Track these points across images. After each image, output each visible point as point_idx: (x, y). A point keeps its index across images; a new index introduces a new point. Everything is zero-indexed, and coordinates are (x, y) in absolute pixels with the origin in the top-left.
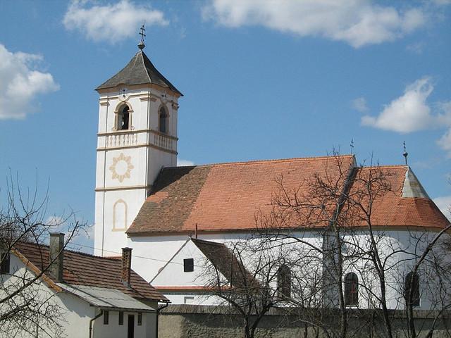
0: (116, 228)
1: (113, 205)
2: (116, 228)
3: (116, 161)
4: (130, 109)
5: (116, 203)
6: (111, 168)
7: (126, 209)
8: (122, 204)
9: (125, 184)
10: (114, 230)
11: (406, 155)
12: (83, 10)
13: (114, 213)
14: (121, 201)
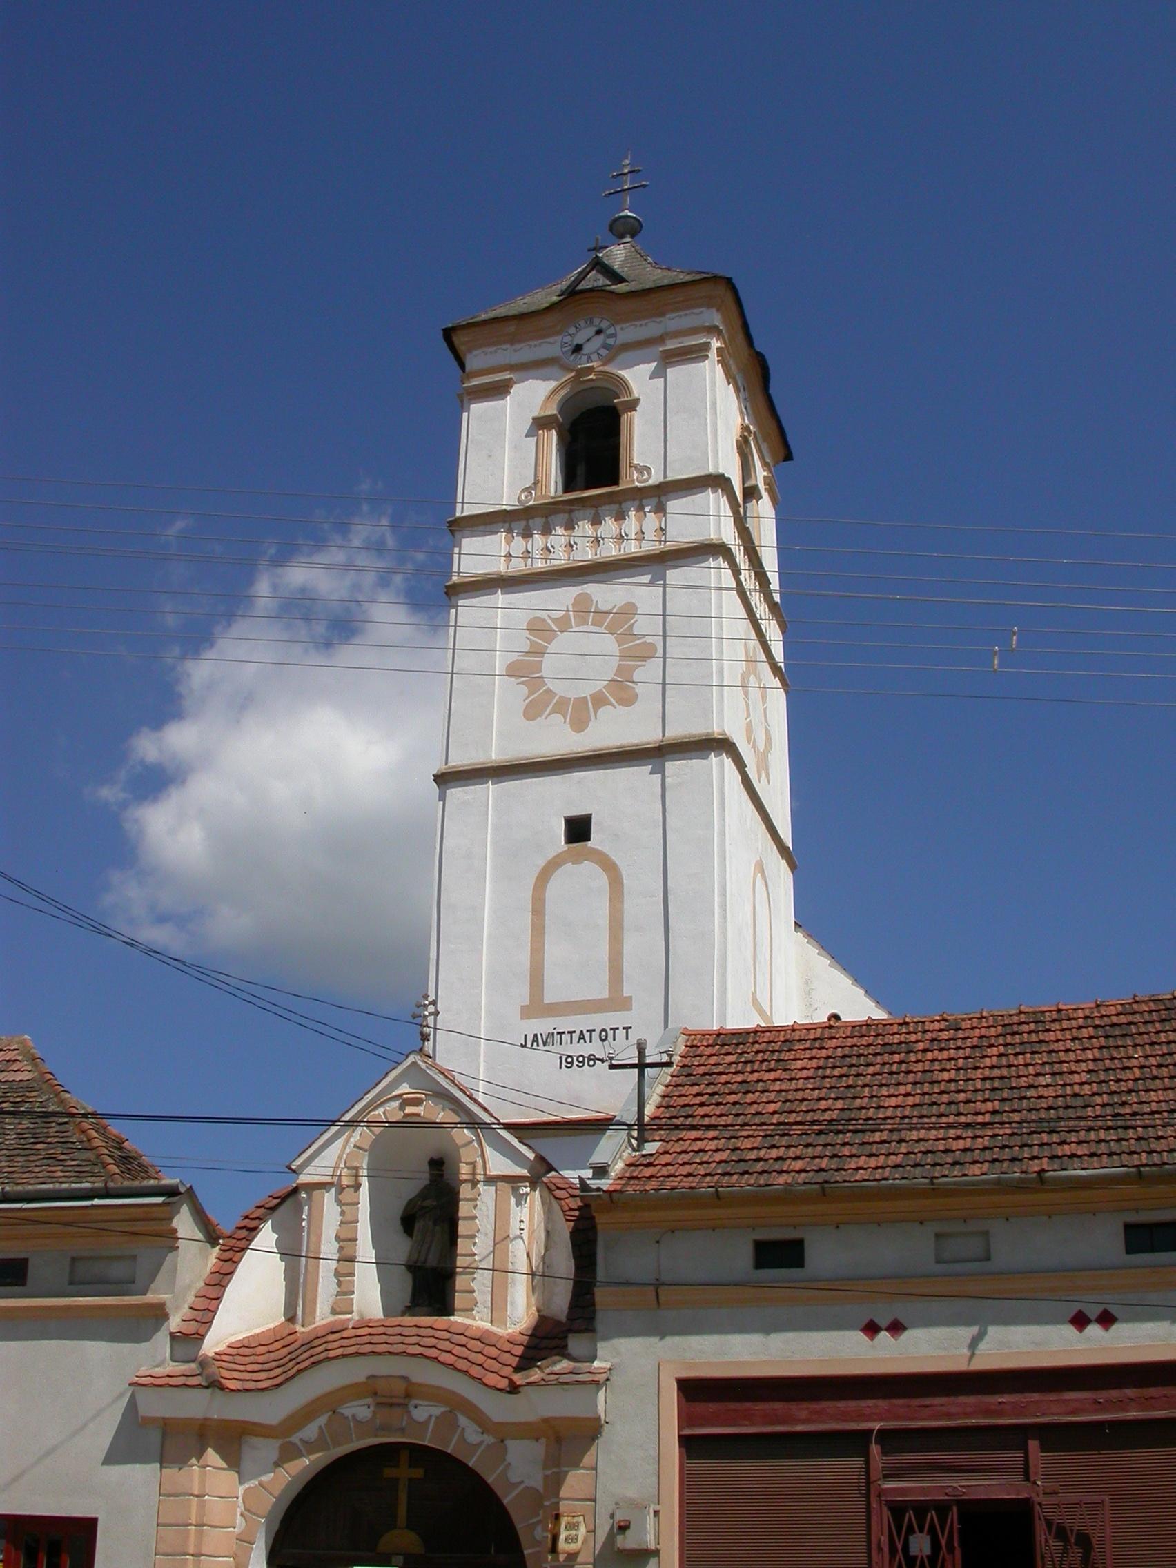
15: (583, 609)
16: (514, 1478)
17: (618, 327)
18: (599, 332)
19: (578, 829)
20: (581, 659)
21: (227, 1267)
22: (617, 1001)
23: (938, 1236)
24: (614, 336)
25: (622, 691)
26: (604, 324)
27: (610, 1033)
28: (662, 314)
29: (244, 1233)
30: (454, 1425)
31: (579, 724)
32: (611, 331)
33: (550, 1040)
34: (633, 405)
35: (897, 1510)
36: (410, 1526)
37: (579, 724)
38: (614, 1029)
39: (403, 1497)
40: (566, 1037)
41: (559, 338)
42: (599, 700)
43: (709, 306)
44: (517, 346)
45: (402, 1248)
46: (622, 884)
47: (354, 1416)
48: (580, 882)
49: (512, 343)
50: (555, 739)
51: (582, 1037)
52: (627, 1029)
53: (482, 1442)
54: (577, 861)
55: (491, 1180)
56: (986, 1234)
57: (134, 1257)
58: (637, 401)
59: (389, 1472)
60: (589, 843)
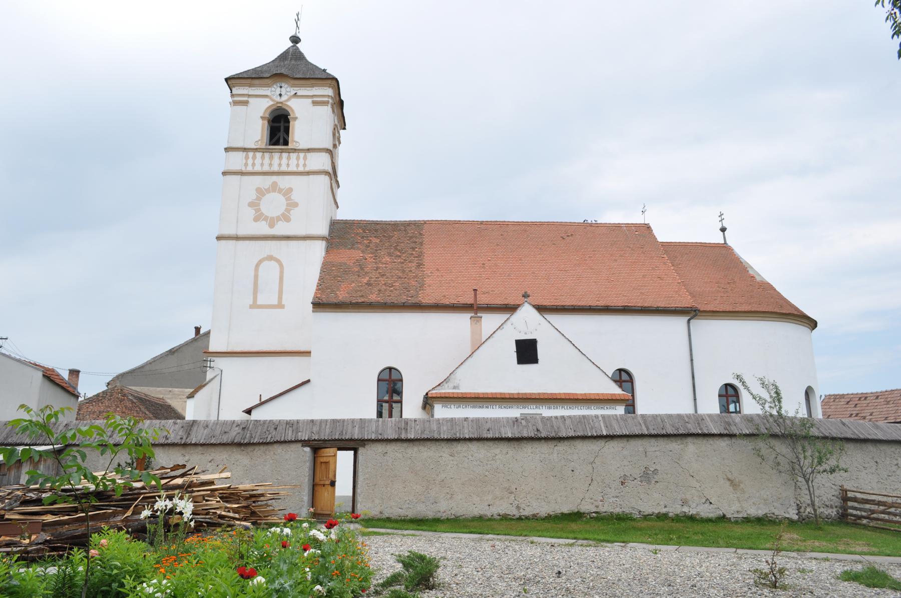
0: (259, 302)
1: (256, 262)
2: (259, 302)
3: (261, 192)
4: (292, 116)
5: (257, 266)
6: (272, 226)
7: (282, 272)
8: (273, 263)
9: (281, 229)
10: (254, 306)
11: (723, 230)
12: (582, 511)
13: (256, 277)
14: (270, 258)
31: (272, 226)
34: (296, 118)
42: (278, 219)
50: (262, 229)
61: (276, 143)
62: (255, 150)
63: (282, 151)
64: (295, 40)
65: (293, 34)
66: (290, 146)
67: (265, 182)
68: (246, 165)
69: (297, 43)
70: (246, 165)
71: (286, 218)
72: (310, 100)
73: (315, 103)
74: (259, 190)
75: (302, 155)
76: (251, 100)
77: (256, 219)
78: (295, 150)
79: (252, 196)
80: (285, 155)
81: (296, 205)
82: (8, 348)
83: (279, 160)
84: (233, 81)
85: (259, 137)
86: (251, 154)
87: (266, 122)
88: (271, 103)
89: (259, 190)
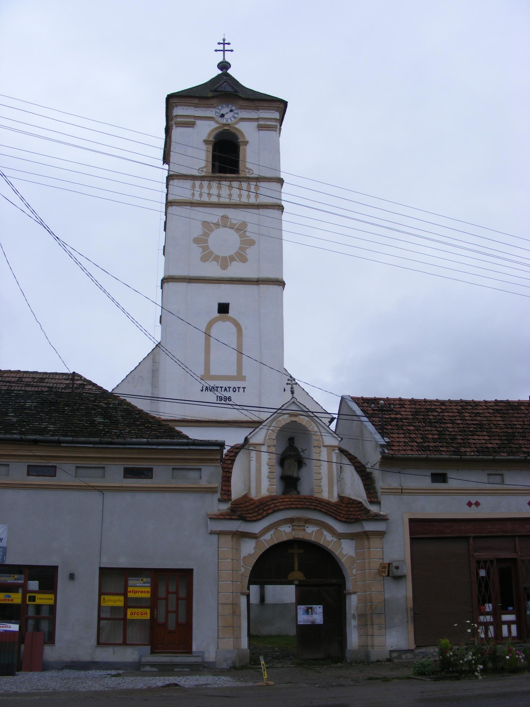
4: (241, 140)
9: (236, 270)
15: (225, 222)
16: (344, 553)
17: (239, 111)
18: (231, 111)
19: (223, 308)
20: (225, 241)
21: (228, 475)
22: (240, 377)
23: (77, 467)
24: (237, 114)
25: (241, 257)
26: (233, 108)
27: (237, 389)
28: (258, 110)
29: (230, 462)
30: (322, 534)
31: (224, 266)
32: (236, 111)
33: (213, 389)
34: (246, 143)
35: (478, 562)
36: (300, 570)
37: (224, 266)
38: (239, 388)
39: (296, 560)
40: (219, 389)
41: (214, 110)
42: (232, 259)
43: (277, 111)
44: (197, 109)
45: (278, 471)
46: (242, 332)
47: (284, 531)
48: (223, 330)
49: (195, 107)
50: (212, 270)
51: (226, 389)
52: (244, 388)
53: (333, 540)
54: (224, 321)
55: (325, 446)
56: (502, 475)
57: (200, 469)
58: (247, 142)
59: (290, 551)
60: (229, 315)
61: (222, 170)
62: (202, 178)
63: (231, 180)
64: (224, 66)
65: (221, 60)
66: (242, 174)
67: (214, 215)
68: (193, 195)
69: (227, 69)
70: (193, 195)
71: (241, 256)
72: (255, 124)
73: (261, 128)
74: (205, 224)
75: (253, 185)
76: (198, 122)
77: (204, 259)
78: (249, 179)
79: (198, 231)
80: (235, 184)
81: (197, 241)
82: (11, 560)
83: (225, 191)
84: (175, 100)
85: (203, 164)
86: (198, 183)
87: (210, 148)
88: (216, 125)
89: (205, 224)
